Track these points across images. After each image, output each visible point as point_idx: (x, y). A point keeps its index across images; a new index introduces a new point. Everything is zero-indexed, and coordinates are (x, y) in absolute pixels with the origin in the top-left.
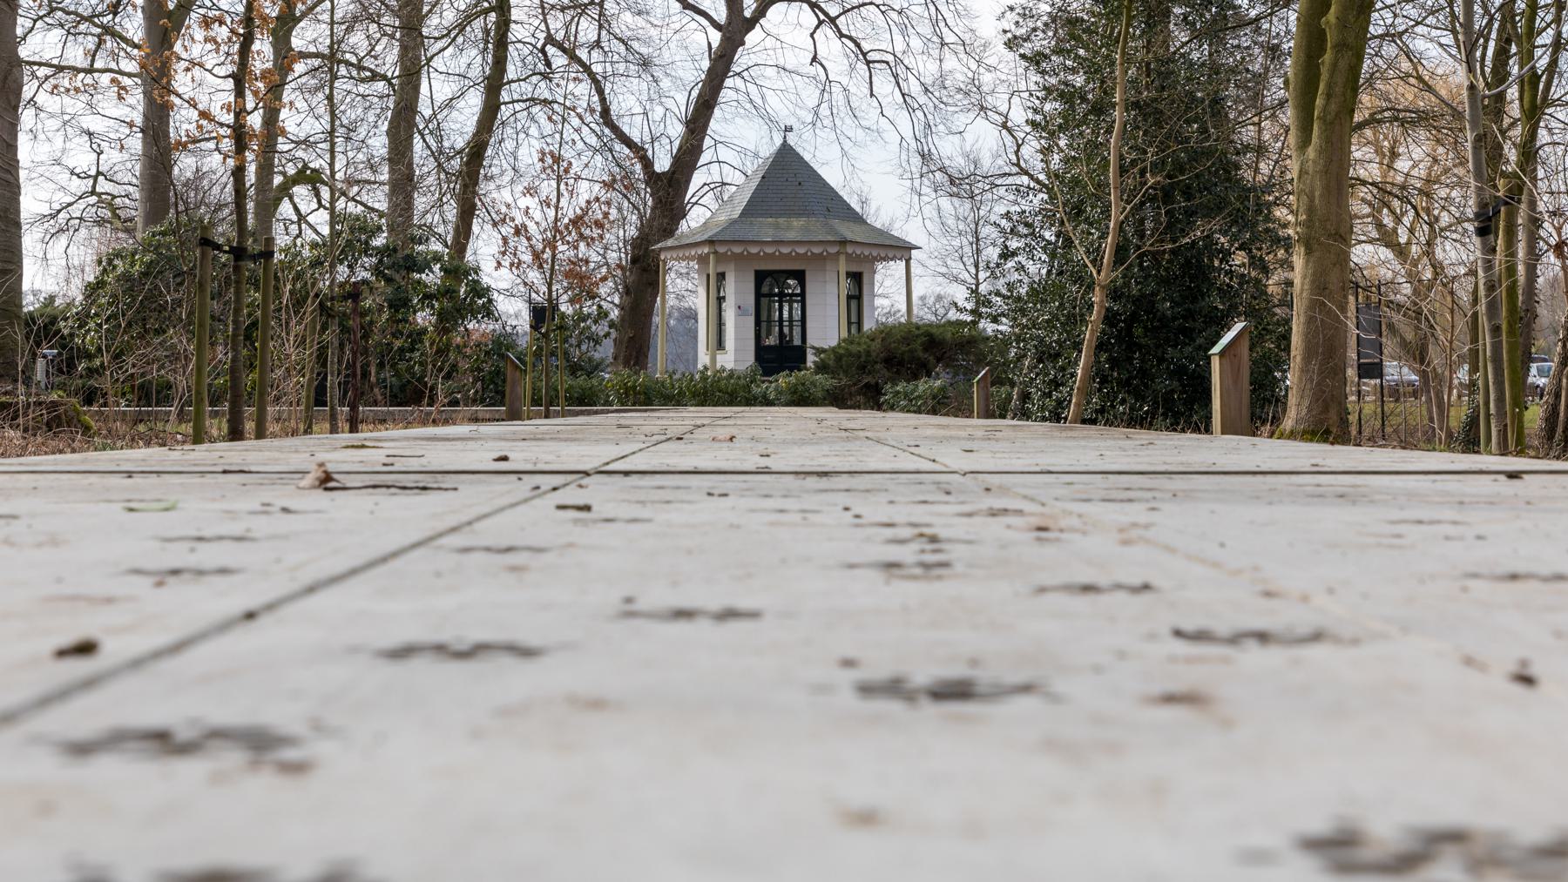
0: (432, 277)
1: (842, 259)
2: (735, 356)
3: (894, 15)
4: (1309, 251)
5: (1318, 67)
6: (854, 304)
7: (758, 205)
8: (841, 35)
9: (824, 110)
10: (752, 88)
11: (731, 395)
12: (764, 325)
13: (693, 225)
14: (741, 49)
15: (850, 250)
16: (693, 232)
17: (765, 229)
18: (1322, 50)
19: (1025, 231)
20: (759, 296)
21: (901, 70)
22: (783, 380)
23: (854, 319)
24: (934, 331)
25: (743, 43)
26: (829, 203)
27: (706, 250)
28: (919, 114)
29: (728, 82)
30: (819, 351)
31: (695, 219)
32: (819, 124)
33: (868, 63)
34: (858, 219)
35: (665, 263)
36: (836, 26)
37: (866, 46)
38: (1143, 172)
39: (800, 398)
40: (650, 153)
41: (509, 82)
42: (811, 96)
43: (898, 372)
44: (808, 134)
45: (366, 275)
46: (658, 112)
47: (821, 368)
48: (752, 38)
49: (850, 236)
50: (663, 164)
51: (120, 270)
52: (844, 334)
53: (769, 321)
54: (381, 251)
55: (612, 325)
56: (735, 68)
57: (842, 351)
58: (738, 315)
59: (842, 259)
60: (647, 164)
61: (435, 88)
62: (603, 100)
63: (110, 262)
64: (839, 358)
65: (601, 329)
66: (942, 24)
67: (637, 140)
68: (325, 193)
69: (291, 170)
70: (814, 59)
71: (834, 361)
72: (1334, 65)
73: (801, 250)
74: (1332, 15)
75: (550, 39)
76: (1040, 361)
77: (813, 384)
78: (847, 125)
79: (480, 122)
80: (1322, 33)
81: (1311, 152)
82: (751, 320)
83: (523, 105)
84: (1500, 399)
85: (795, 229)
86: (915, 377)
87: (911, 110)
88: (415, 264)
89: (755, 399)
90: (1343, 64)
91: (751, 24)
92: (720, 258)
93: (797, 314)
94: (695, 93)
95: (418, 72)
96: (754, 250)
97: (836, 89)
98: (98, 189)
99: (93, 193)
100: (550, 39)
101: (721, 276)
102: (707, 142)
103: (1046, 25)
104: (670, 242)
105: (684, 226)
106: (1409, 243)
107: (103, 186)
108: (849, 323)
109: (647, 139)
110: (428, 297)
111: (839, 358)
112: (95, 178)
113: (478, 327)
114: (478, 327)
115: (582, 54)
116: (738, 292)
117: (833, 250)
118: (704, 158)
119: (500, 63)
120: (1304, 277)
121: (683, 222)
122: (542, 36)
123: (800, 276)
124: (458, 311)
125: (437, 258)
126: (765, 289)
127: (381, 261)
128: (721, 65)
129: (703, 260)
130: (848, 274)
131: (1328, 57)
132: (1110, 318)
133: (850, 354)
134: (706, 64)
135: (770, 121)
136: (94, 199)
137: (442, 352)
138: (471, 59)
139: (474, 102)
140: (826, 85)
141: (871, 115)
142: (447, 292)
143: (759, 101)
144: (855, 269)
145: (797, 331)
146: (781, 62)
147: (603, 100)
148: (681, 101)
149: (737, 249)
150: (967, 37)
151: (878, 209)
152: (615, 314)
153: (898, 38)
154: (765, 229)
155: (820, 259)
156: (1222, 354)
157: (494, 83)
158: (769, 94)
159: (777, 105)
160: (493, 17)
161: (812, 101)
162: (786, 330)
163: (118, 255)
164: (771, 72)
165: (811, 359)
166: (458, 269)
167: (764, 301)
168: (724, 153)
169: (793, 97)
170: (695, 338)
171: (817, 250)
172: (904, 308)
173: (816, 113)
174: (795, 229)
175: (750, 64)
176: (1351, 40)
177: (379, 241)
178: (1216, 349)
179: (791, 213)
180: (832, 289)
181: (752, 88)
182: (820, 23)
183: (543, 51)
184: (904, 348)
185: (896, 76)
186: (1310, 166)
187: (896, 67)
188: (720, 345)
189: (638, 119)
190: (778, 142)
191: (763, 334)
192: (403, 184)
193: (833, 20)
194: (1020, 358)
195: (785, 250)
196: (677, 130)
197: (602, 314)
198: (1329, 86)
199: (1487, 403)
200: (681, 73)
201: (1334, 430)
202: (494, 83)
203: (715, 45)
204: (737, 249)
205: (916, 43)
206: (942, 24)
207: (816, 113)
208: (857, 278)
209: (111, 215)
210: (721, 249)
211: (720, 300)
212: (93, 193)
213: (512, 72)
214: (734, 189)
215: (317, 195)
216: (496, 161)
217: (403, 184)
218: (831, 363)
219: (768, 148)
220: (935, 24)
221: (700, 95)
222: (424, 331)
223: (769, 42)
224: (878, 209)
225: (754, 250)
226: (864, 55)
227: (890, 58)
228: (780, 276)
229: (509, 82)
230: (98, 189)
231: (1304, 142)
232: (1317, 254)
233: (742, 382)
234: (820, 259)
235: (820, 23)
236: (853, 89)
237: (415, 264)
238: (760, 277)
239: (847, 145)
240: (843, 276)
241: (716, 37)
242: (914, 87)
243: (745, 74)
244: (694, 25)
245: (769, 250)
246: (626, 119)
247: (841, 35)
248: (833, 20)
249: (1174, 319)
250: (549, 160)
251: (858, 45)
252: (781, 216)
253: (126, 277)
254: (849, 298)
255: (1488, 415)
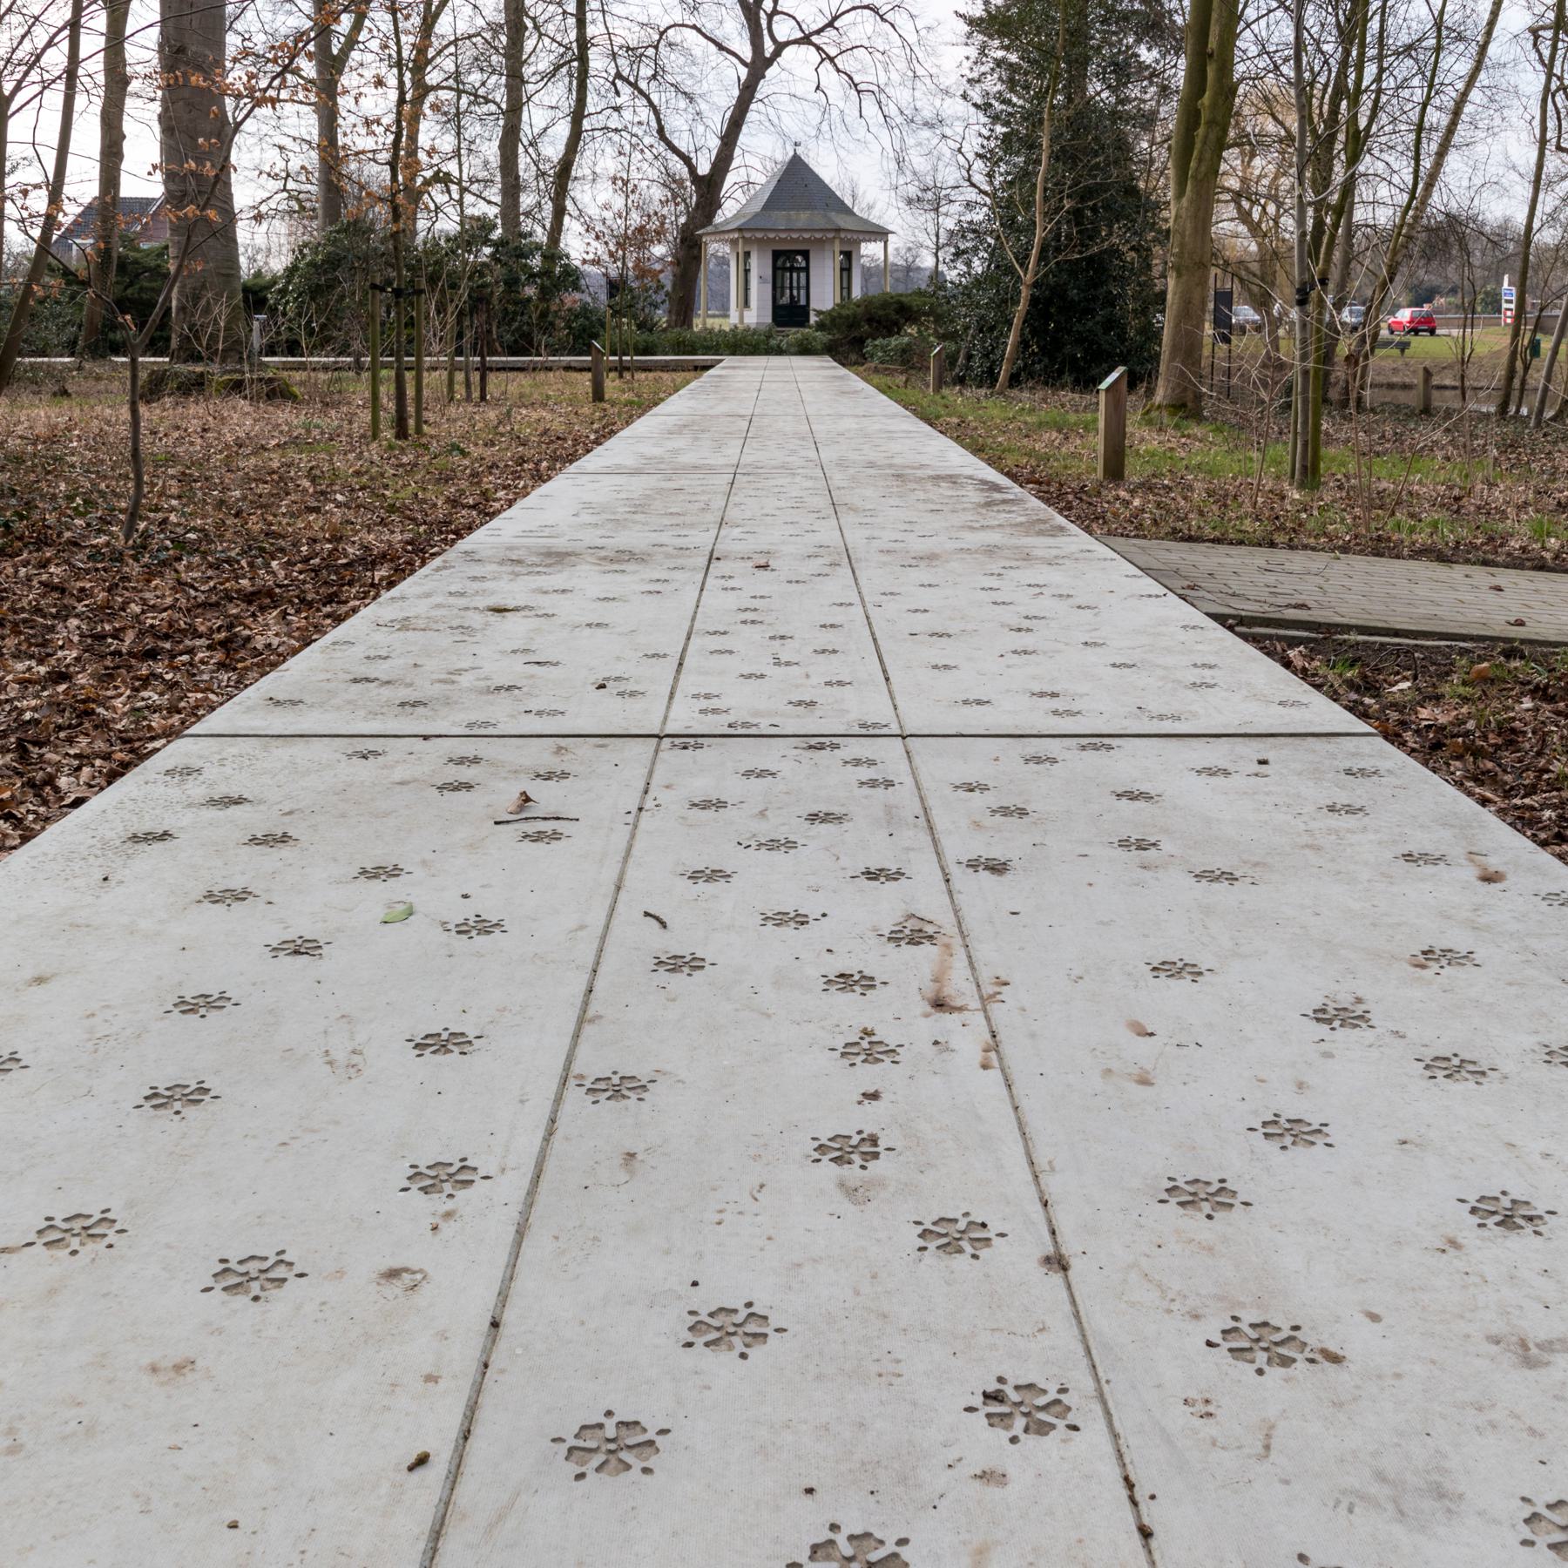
0: (536, 262)
1: (837, 242)
2: (756, 315)
3: (879, 55)
4: (1179, 275)
5: (1193, 137)
6: (845, 274)
7: (773, 202)
8: (838, 71)
9: (825, 127)
10: (770, 111)
11: (754, 347)
12: (779, 290)
13: (729, 215)
14: (762, 81)
15: (843, 235)
16: (727, 222)
17: (780, 219)
18: (1197, 125)
19: (972, 236)
20: (775, 269)
21: (883, 98)
22: (794, 334)
23: (845, 285)
24: (903, 299)
25: (764, 77)
26: (831, 200)
27: (736, 236)
28: (896, 131)
29: (753, 106)
30: (819, 313)
31: (732, 205)
32: (821, 137)
33: (859, 92)
34: (849, 212)
35: (706, 244)
36: (835, 65)
37: (857, 79)
38: (1061, 200)
39: (805, 350)
40: (694, 161)
41: (589, 115)
42: (815, 115)
43: (877, 329)
44: (812, 144)
45: (485, 259)
46: (701, 129)
47: (821, 326)
48: (771, 72)
49: (843, 225)
50: (704, 168)
51: (309, 258)
52: (838, 301)
53: (783, 288)
54: (495, 244)
55: (667, 294)
56: (758, 96)
57: (835, 314)
58: (759, 283)
59: (837, 242)
60: (692, 169)
61: (534, 117)
62: (659, 120)
63: (301, 252)
64: (833, 320)
65: (659, 298)
66: (915, 62)
67: (683, 150)
68: (454, 188)
69: (428, 174)
70: (818, 88)
71: (830, 321)
72: (1206, 137)
73: (807, 236)
74: (1206, 99)
75: (619, 75)
76: (981, 331)
77: (815, 339)
78: (843, 137)
79: (568, 145)
80: (1197, 113)
81: (1185, 201)
82: (769, 287)
83: (601, 133)
84: (1305, 423)
85: (803, 218)
86: (890, 334)
87: (890, 128)
88: (521, 254)
89: (772, 349)
90: (1212, 136)
91: (769, 62)
92: (746, 241)
93: (803, 282)
94: (728, 115)
95: (520, 109)
96: (772, 235)
97: (835, 113)
98: (288, 187)
99: (284, 190)
100: (619, 75)
101: (747, 255)
102: (737, 152)
103: (993, 69)
104: (709, 229)
105: (719, 218)
106: (1260, 221)
107: (291, 185)
108: (842, 288)
109: (692, 148)
110: (533, 276)
111: (833, 320)
112: (286, 179)
113: (571, 299)
114: (571, 299)
115: (643, 85)
116: (760, 266)
117: (830, 235)
118: (734, 164)
119: (581, 101)
120: (1175, 294)
121: (720, 212)
122: (613, 72)
123: (806, 255)
124: (555, 286)
125: (538, 247)
126: (779, 263)
127: (497, 251)
128: (747, 93)
129: (734, 242)
130: (841, 253)
131: (1201, 131)
132: (1034, 301)
133: (840, 316)
134: (736, 93)
135: (783, 135)
136: (285, 195)
137: (544, 315)
138: (558, 94)
139: (563, 130)
140: (825, 110)
141: (861, 133)
142: (546, 273)
143: (776, 121)
144: (846, 249)
145: (803, 292)
146: (793, 92)
147: (659, 120)
148: (717, 121)
149: (759, 235)
150: (933, 71)
151: (865, 192)
152: (669, 288)
153: (881, 73)
154: (780, 219)
155: (821, 242)
156: (1108, 390)
157: (578, 115)
158: (783, 114)
159: (790, 124)
160: (575, 64)
161: (815, 122)
162: (795, 292)
163: (305, 245)
164: (785, 98)
165: (813, 319)
166: (552, 252)
167: (779, 273)
168: (750, 160)
169: (801, 118)
170: (728, 278)
171: (818, 235)
172: (882, 258)
173: (819, 129)
174: (803, 218)
175: (770, 92)
176: (1219, 118)
177: (497, 234)
178: (1104, 386)
179: (798, 208)
180: (829, 263)
181: (770, 111)
182: (823, 60)
183: (613, 83)
184: (881, 313)
185: (879, 103)
186: (1183, 213)
187: (878, 94)
188: (746, 304)
189: (686, 135)
190: (791, 153)
191: (778, 295)
192: (512, 188)
193: (832, 60)
194: (966, 328)
195: (795, 236)
196: (714, 143)
197: (660, 287)
198: (1201, 153)
199: (1296, 422)
200: (716, 99)
201: (1189, 404)
202: (578, 115)
203: (743, 78)
204: (759, 235)
205: (895, 77)
206: (915, 62)
207: (819, 129)
208: (848, 255)
209: (299, 209)
210: (748, 235)
211: (747, 271)
212: (284, 190)
213: (590, 108)
214: (758, 187)
215: (449, 192)
216: (581, 168)
217: (512, 188)
218: (827, 322)
219: (783, 155)
220: (910, 61)
221: (732, 116)
222: (529, 300)
223: (784, 75)
224: (865, 192)
225: (772, 235)
226: (856, 85)
227: (875, 89)
228: (790, 254)
229: (589, 115)
230: (288, 187)
231: (1180, 194)
232: (1185, 278)
233: (763, 337)
234: (820, 241)
235: (823, 60)
236: (846, 111)
237: (521, 254)
238: (776, 255)
239: (842, 153)
240: (837, 253)
241: (743, 72)
242: (892, 110)
243: (766, 100)
244: (727, 63)
245: (783, 235)
246: (677, 134)
247: (838, 71)
248: (832, 60)
249: (1080, 301)
250: (620, 183)
251: (851, 78)
252: (793, 209)
253: (312, 264)
254: (842, 270)
255: (1333, 237)
